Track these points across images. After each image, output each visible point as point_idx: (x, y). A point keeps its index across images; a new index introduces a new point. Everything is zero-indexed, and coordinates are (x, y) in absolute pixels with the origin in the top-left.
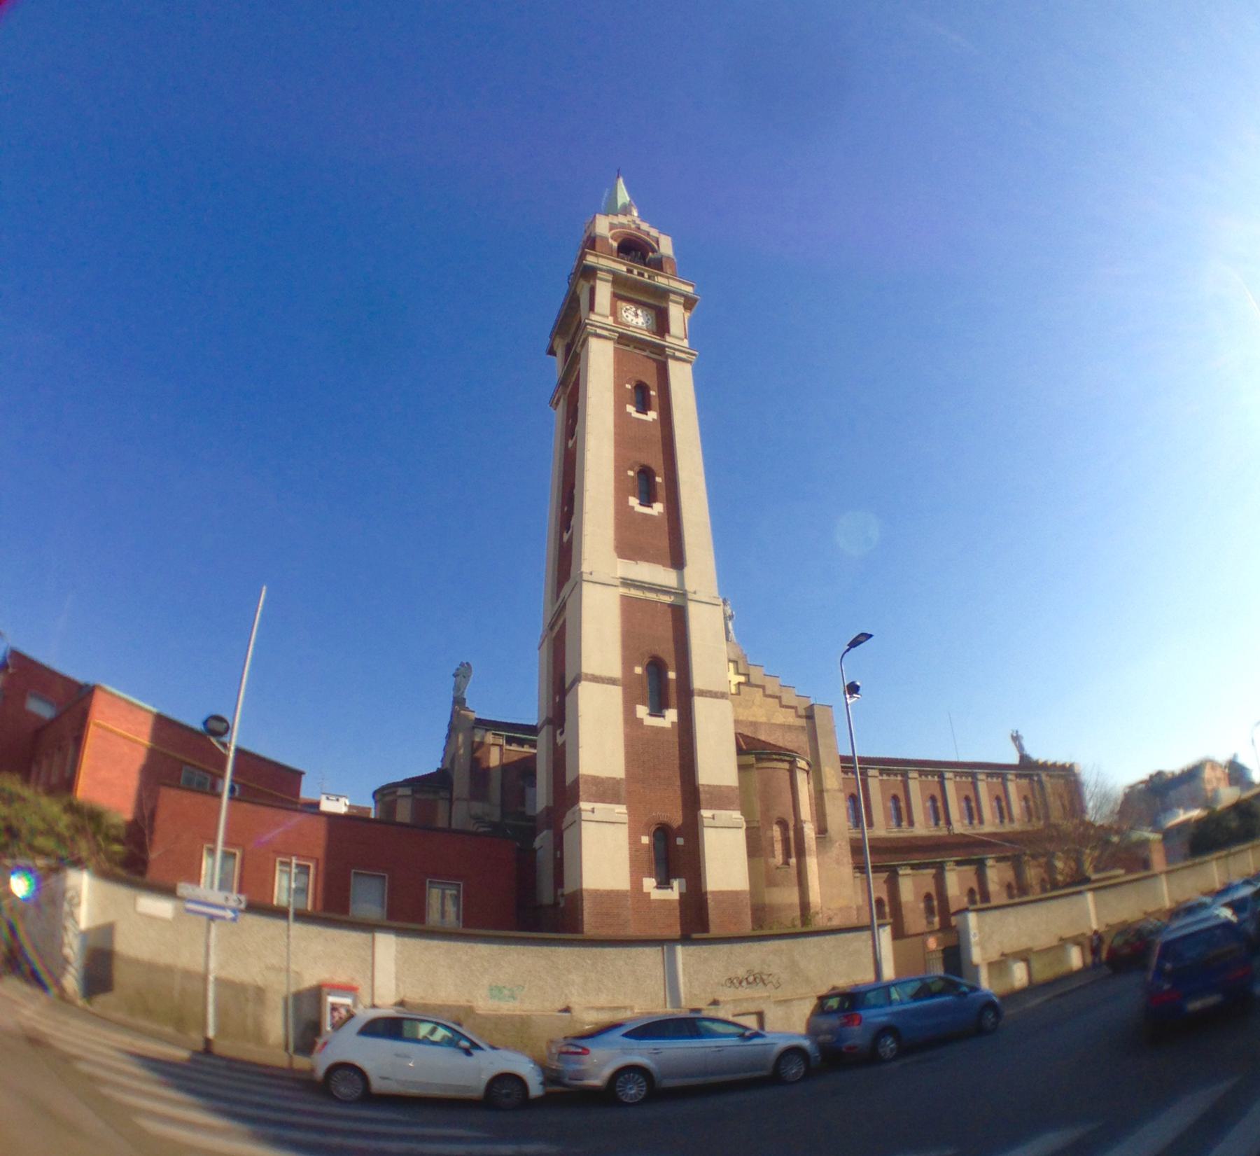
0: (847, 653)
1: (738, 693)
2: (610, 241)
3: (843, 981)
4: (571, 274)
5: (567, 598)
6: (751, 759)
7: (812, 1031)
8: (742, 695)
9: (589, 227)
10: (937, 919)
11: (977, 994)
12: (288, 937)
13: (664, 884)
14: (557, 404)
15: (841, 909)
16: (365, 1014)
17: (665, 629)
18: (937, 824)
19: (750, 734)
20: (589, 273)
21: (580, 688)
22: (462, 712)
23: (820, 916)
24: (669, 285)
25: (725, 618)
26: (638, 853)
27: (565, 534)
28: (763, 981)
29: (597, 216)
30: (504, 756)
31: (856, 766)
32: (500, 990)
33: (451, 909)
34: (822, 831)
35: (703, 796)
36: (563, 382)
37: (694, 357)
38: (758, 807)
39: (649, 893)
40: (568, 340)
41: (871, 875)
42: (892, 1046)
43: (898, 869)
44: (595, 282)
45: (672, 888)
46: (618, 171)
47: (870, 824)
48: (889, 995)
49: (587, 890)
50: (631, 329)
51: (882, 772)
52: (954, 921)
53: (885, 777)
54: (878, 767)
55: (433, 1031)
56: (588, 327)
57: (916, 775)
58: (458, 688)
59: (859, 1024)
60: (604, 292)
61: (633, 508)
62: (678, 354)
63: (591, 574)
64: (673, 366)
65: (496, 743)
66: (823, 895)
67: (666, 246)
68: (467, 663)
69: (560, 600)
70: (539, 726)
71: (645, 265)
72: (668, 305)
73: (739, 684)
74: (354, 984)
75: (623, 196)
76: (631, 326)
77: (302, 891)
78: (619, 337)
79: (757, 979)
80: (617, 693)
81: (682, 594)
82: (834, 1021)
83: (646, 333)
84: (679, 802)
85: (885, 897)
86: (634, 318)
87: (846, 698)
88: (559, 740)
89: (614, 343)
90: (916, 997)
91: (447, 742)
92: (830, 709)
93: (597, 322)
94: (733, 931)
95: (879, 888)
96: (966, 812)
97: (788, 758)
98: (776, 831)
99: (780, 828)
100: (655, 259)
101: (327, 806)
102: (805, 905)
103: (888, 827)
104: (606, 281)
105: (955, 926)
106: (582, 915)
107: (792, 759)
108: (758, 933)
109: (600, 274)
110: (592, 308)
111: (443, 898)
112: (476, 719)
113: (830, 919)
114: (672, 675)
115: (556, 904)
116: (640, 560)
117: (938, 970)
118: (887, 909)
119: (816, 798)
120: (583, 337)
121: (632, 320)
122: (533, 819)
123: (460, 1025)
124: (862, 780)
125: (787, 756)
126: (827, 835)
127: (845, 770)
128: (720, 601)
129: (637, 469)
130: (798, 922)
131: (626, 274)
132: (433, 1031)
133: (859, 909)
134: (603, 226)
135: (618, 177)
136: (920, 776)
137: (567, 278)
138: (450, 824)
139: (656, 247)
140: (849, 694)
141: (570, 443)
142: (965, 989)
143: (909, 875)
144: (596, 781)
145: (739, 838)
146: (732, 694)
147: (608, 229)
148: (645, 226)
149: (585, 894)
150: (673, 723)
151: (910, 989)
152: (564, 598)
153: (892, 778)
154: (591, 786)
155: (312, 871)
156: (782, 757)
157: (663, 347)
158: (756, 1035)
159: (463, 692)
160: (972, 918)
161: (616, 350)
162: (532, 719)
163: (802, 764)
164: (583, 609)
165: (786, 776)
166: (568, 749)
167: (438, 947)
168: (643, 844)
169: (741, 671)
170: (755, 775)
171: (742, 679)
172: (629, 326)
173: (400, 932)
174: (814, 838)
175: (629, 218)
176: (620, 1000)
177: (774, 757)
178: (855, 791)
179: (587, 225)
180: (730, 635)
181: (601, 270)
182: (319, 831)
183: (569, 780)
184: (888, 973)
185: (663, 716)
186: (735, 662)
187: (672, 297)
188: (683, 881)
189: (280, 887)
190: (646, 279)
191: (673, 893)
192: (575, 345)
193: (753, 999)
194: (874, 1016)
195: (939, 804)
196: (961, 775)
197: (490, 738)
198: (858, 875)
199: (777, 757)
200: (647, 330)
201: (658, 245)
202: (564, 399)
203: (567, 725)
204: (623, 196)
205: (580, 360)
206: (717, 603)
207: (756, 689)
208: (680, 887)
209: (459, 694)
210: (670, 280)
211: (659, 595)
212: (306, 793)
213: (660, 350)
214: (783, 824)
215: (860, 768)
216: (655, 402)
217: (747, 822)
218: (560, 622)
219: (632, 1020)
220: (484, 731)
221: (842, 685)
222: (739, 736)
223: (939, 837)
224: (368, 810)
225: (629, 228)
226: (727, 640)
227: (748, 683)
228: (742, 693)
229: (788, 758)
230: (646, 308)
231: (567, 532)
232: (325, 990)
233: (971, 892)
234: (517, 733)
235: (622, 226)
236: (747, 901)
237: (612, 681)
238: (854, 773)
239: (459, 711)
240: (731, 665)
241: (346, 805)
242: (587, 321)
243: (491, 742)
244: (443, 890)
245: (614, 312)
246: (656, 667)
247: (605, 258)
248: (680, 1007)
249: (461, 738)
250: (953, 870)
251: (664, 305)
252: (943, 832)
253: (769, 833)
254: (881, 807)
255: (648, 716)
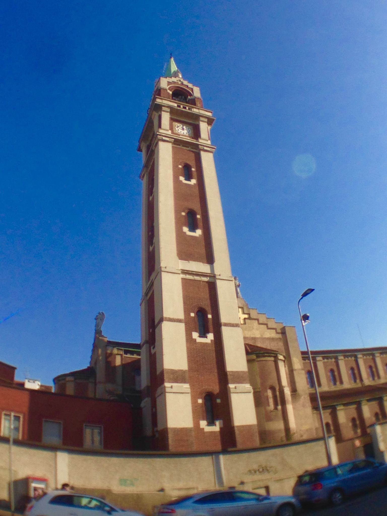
0: (301, 300)
1: (245, 323)
2: (168, 91)
3: (311, 466)
4: (149, 109)
5: (154, 280)
6: (254, 357)
7: (296, 493)
8: (247, 324)
9: (157, 84)
10: (359, 431)
11: (383, 467)
12: (10, 452)
13: (211, 423)
14: (143, 177)
15: (307, 430)
16: (52, 493)
17: (205, 294)
18: (355, 381)
19: (252, 344)
20: (158, 108)
21: (163, 325)
22: (100, 338)
23: (296, 435)
24: (199, 113)
25: (236, 287)
26: (196, 408)
27: (151, 247)
28: (268, 470)
29: (161, 78)
30: (123, 360)
31: (309, 356)
32: (125, 481)
33: (97, 438)
34: (294, 391)
35: (229, 377)
36: (146, 166)
37: (214, 150)
38: (259, 381)
39: (203, 429)
40: (148, 143)
41: (322, 412)
42: (340, 497)
43: (336, 407)
44: (161, 112)
45: (215, 425)
46: (171, 54)
47: (320, 385)
48: (336, 472)
49: (170, 428)
50: (181, 136)
51: (324, 358)
52: (369, 430)
53: (326, 360)
54: (321, 355)
55: (90, 502)
56: (158, 136)
57: (342, 358)
58: (97, 325)
59: (321, 488)
60: (166, 117)
61: (185, 233)
62: (205, 148)
63: (166, 268)
64: (203, 154)
65: (119, 353)
66: (297, 424)
67: (197, 92)
68: (102, 313)
69: (150, 282)
70: (142, 344)
71: (187, 103)
72: (199, 123)
73: (245, 319)
74: (46, 478)
75: (174, 67)
76: (181, 135)
77: (17, 429)
78: (174, 141)
79: (264, 469)
80: (182, 326)
81: (213, 276)
82: (307, 488)
83: (189, 138)
84: (217, 381)
85: (330, 422)
86: (182, 131)
87: (302, 322)
88: (153, 351)
89: (172, 144)
90: (351, 471)
91: (92, 353)
92: (293, 328)
93: (163, 133)
94: (250, 446)
95: (326, 417)
96: (370, 374)
97: (273, 355)
98: (270, 393)
99: (271, 391)
100: (192, 99)
101: (29, 385)
102: (287, 429)
103: (329, 385)
104: (167, 112)
105: (369, 434)
106: (168, 441)
107: (276, 355)
108: (263, 446)
109: (164, 108)
110: (160, 126)
111: (93, 433)
112: (108, 341)
113: (302, 436)
114: (210, 316)
115: (154, 436)
116: (191, 260)
117: (362, 456)
118: (332, 428)
119: (290, 374)
120: (156, 141)
121: (181, 132)
122: (140, 392)
123: (104, 499)
124: (313, 363)
125: (273, 354)
126: (297, 393)
127: (304, 359)
128: (233, 279)
129: (187, 211)
130: (284, 439)
131: (177, 108)
132: (90, 502)
133: (317, 429)
134: (164, 83)
135: (171, 58)
136: (345, 358)
137: (147, 111)
138: (95, 395)
139: (192, 93)
140: (304, 320)
141: (151, 198)
142: (377, 465)
143: (342, 409)
144: (173, 372)
145: (250, 398)
146: (241, 324)
147: (167, 85)
148: (185, 83)
149: (169, 430)
150: (211, 340)
151: (347, 468)
152: (152, 280)
153: (330, 360)
154: (170, 375)
155: (21, 419)
156: (270, 354)
157: (197, 145)
158: (266, 498)
159: (100, 327)
160: (378, 429)
161: (173, 147)
162: (138, 341)
163: (281, 357)
164: (163, 285)
165: (273, 364)
166: (157, 356)
167: (91, 460)
168: (199, 403)
169: (246, 312)
170: (256, 365)
171: (246, 316)
172: (179, 135)
173: (70, 451)
174: (290, 395)
175: (177, 79)
176: (191, 485)
177: (266, 355)
178: (310, 369)
179: (156, 83)
180: (239, 295)
181: (164, 106)
182: (25, 399)
183: (158, 372)
184: (335, 460)
185: (206, 337)
186: (242, 308)
187: (201, 119)
188: (221, 421)
189: (4, 426)
190: (187, 110)
191: (216, 428)
192: (152, 146)
193: (262, 480)
194: (328, 484)
195: (356, 371)
196: (327, 358)
197: (115, 351)
198: (315, 412)
199: (267, 355)
200: (190, 137)
201: (193, 92)
202: (147, 175)
203: (156, 344)
204: (174, 67)
205: (154, 154)
206: (231, 280)
207: (254, 321)
208: (220, 424)
209: (99, 328)
210: (200, 110)
211: (201, 277)
212: (17, 378)
213: (196, 146)
214: (273, 388)
215: (312, 357)
216: (195, 174)
217: (254, 389)
218: (151, 292)
219: (197, 494)
220: (112, 347)
221: (300, 316)
222: (246, 345)
223: (357, 389)
224: (50, 388)
225: (177, 83)
226: (237, 297)
227: (250, 318)
228: (246, 323)
229: (273, 355)
230: (188, 125)
231: (152, 246)
232: (30, 480)
233: (376, 415)
234: (130, 348)
235: (174, 82)
236: (256, 430)
237: (179, 321)
238: (309, 360)
239: (99, 337)
240: (240, 310)
241: (38, 385)
242: (158, 133)
243: (116, 353)
244: (93, 429)
245: (171, 128)
246: (201, 313)
247: (165, 100)
248: (223, 487)
249: (100, 351)
250: (366, 404)
251: (197, 123)
252: (359, 385)
253: (265, 394)
254: (324, 376)
255: (198, 337)
